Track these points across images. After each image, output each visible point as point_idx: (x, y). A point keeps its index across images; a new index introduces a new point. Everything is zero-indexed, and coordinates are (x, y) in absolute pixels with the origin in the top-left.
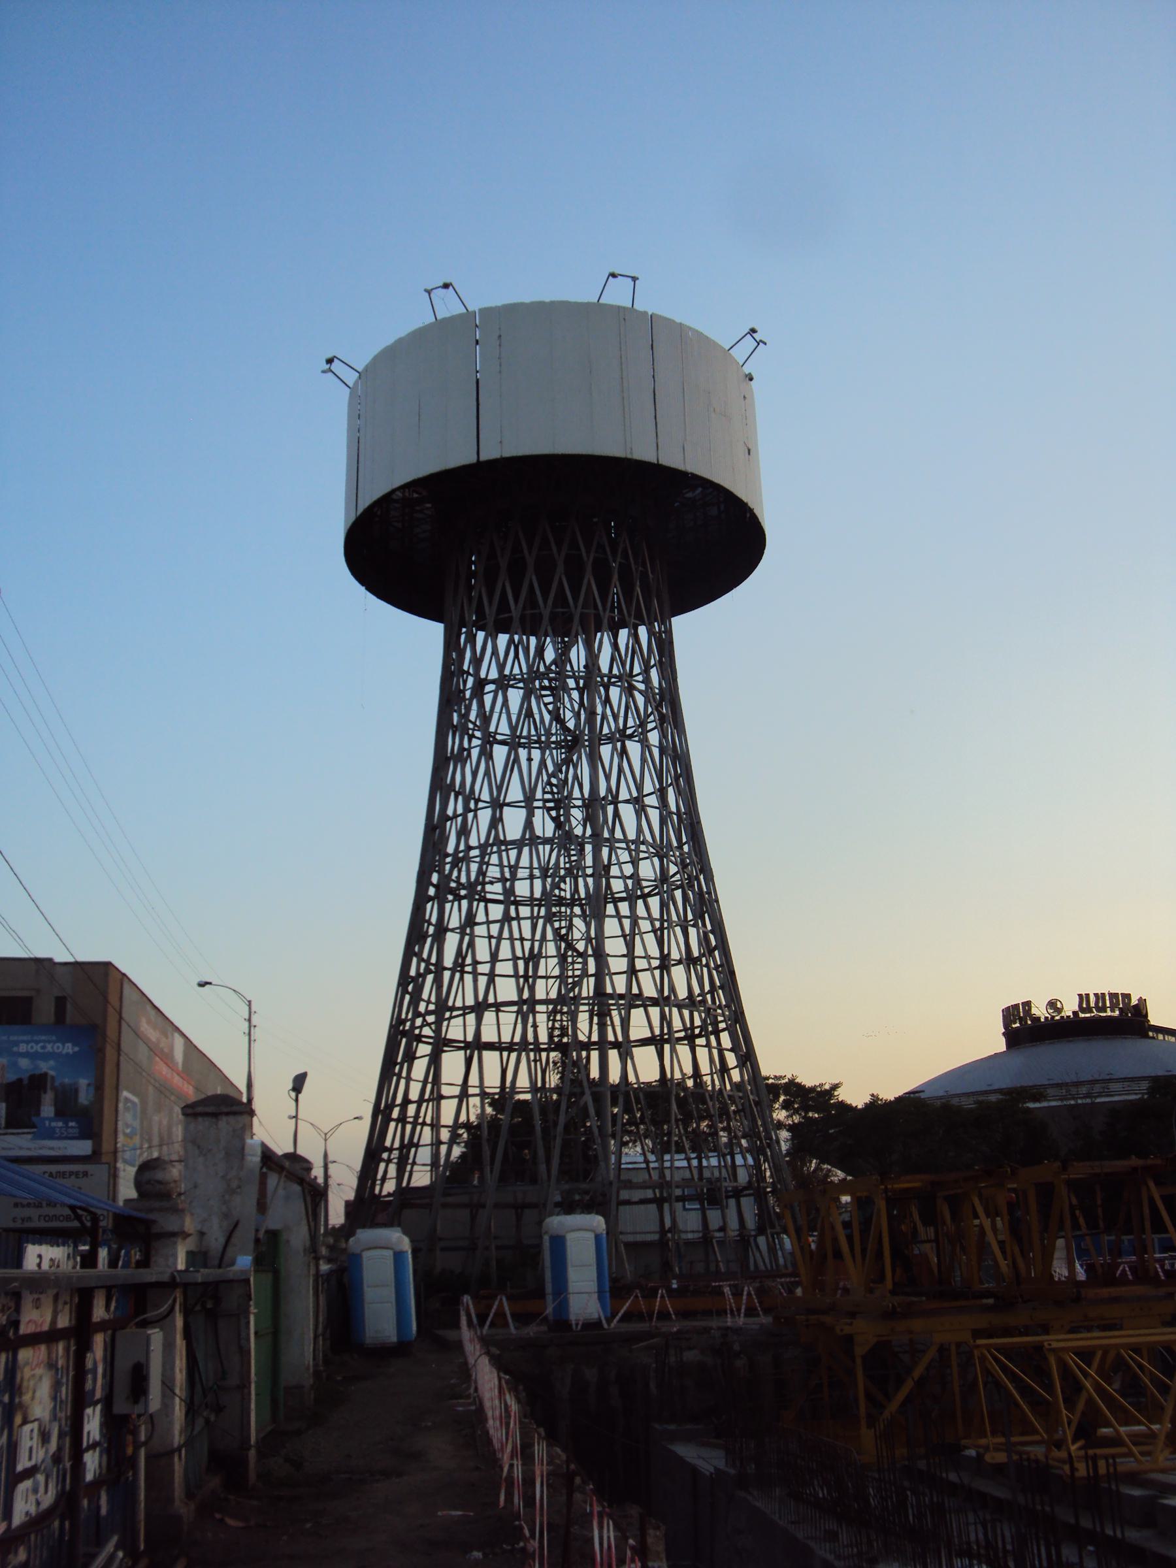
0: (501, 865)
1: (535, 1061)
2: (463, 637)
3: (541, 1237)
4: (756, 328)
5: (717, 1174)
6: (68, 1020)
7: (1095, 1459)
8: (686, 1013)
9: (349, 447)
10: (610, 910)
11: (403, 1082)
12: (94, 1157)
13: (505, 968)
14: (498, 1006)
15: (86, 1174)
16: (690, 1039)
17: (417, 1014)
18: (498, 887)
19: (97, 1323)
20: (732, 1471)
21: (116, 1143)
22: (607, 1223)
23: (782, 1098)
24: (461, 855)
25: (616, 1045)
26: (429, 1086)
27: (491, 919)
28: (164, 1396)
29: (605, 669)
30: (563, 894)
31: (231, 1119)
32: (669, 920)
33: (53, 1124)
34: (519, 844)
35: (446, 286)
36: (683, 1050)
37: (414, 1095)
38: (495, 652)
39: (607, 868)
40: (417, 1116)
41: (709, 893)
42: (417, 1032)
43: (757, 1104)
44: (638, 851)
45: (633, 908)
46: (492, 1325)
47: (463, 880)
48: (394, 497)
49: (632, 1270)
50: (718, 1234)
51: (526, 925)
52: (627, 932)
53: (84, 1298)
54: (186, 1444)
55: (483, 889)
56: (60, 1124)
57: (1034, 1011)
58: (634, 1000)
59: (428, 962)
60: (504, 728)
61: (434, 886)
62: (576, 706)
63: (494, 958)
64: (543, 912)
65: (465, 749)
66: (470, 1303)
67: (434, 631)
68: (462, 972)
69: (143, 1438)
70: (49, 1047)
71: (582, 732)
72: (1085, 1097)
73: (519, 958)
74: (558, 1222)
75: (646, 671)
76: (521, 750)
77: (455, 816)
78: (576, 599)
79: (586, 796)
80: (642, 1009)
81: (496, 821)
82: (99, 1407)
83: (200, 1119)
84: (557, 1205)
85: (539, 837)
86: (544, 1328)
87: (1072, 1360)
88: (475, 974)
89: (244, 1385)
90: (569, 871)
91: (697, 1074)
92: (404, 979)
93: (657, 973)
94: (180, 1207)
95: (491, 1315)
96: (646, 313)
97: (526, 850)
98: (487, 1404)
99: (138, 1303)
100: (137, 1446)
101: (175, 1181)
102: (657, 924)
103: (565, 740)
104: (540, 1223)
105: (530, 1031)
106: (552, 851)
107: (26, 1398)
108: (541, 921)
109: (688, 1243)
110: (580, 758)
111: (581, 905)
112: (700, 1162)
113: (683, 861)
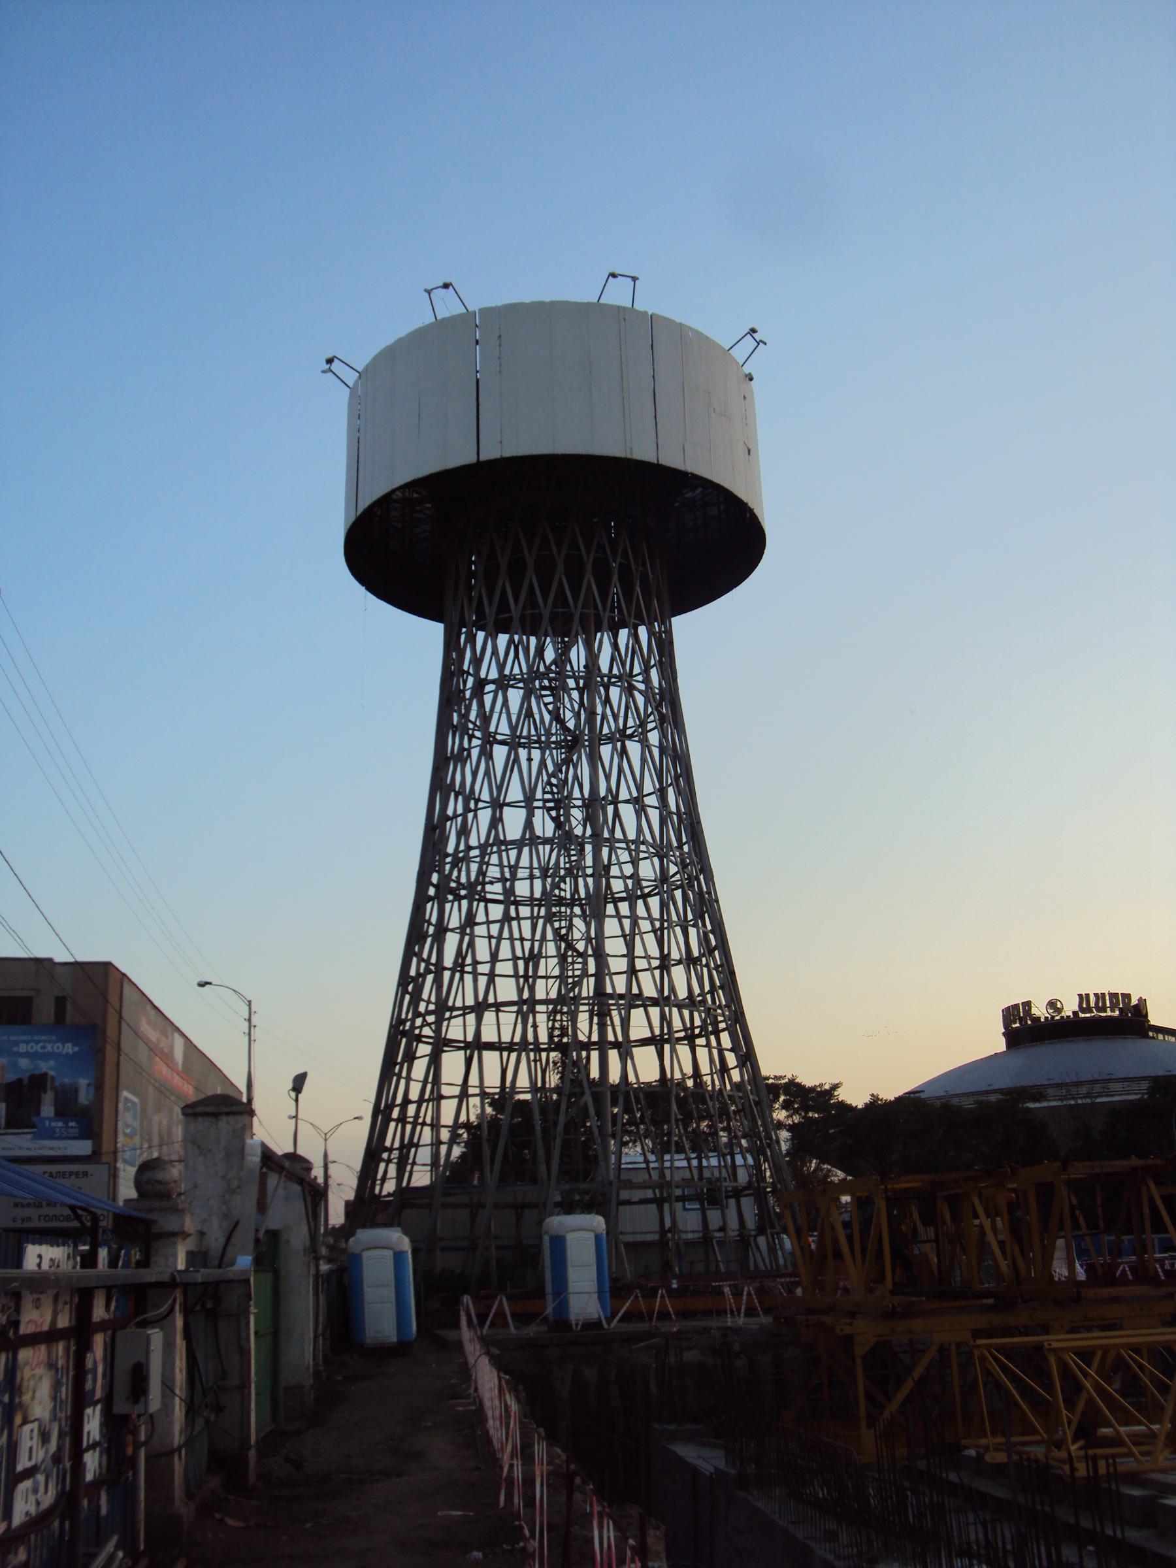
0: (501, 865)
1: (535, 1061)
2: (463, 637)
3: (541, 1237)
4: (756, 328)
5: (717, 1174)
6: (68, 1020)
7: (1095, 1459)
8: (686, 1013)
9: (349, 447)
10: (610, 910)
11: (403, 1082)
12: (94, 1157)
13: (505, 968)
14: (498, 1006)
15: (86, 1174)
16: (690, 1039)
17: (417, 1014)
18: (498, 887)
19: (97, 1323)
20: (732, 1471)
21: (116, 1143)
22: (607, 1223)
23: (782, 1098)
24: (461, 855)
25: (616, 1045)
26: (429, 1086)
27: (491, 919)
28: (164, 1396)
29: (605, 669)
30: (563, 894)
31: (231, 1119)
32: (669, 920)
33: (53, 1124)
34: (519, 844)
35: (446, 286)
36: (683, 1050)
37: (414, 1095)
38: (495, 652)
39: (607, 868)
40: (417, 1116)
41: (709, 893)
42: (417, 1032)
43: (757, 1104)
44: (638, 851)
45: (633, 908)
46: (492, 1325)
47: (463, 880)
48: (394, 497)
49: (632, 1270)
50: (718, 1234)
51: (526, 925)
52: (627, 932)
53: (84, 1298)
54: (186, 1444)
55: (483, 889)
56: (60, 1124)
57: (1034, 1011)
58: (634, 1000)
59: (428, 962)
60: (504, 728)
61: (434, 886)
62: (576, 706)
63: (494, 958)
64: (543, 912)
65: (465, 749)
66: (470, 1303)
67: (434, 631)
68: (462, 972)
69: (143, 1438)
70: (49, 1047)
71: (582, 732)
72: (1085, 1097)
73: (519, 958)
74: (558, 1222)
75: (646, 671)
76: (521, 750)
77: (455, 816)
78: (576, 599)
79: (586, 796)
80: (642, 1009)
81: (496, 821)
82: (99, 1407)
83: (200, 1119)
84: (557, 1205)
85: (539, 837)
86: (544, 1328)
87: (1072, 1360)
88: (475, 974)
89: (244, 1385)
90: (569, 871)
91: (697, 1074)
92: (404, 979)
93: (657, 973)
94: (180, 1207)
95: (491, 1315)
96: (646, 313)
97: (526, 850)
98: (487, 1404)
99: (138, 1303)
100: (137, 1446)
101: (175, 1181)
102: (657, 924)
103: (565, 740)
104: (540, 1223)
105: (530, 1031)
106: (552, 851)
107: (26, 1398)
108: (541, 921)
109: (688, 1243)
110: (580, 758)
111: (581, 905)
112: (700, 1162)
113: (683, 861)
